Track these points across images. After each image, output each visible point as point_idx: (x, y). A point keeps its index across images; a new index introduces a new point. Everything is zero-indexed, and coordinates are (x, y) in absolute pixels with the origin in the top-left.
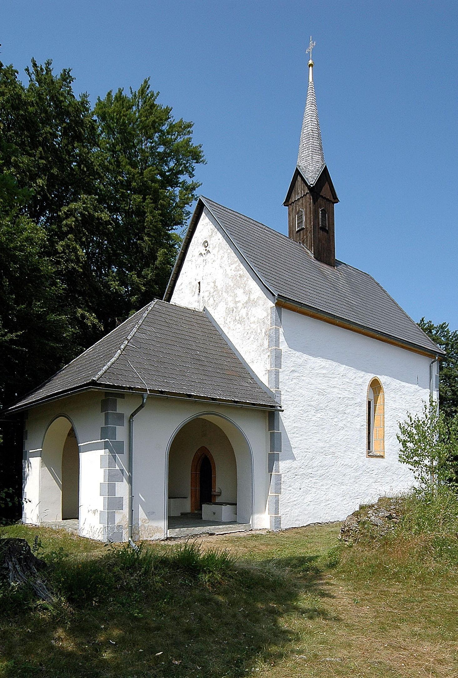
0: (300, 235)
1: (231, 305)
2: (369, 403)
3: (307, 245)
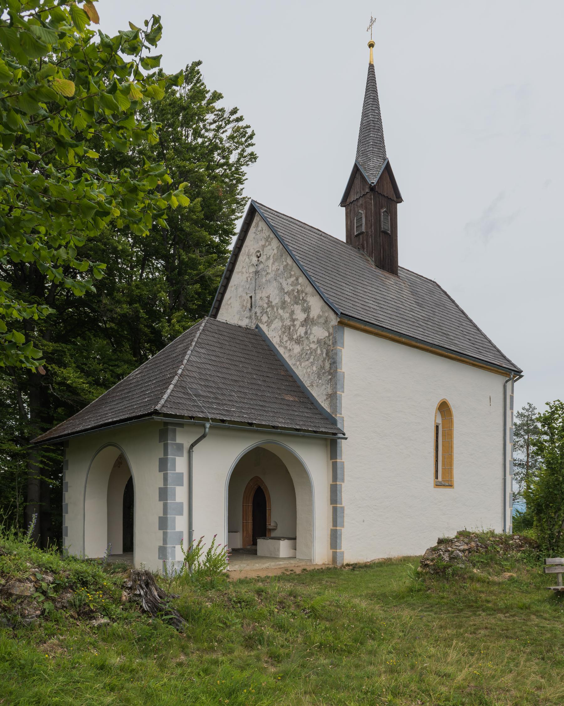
0: (359, 238)
1: (288, 323)
2: (437, 427)
3: (367, 252)
